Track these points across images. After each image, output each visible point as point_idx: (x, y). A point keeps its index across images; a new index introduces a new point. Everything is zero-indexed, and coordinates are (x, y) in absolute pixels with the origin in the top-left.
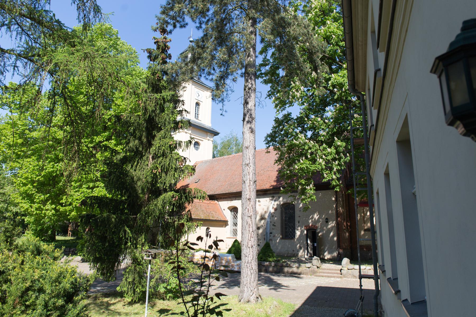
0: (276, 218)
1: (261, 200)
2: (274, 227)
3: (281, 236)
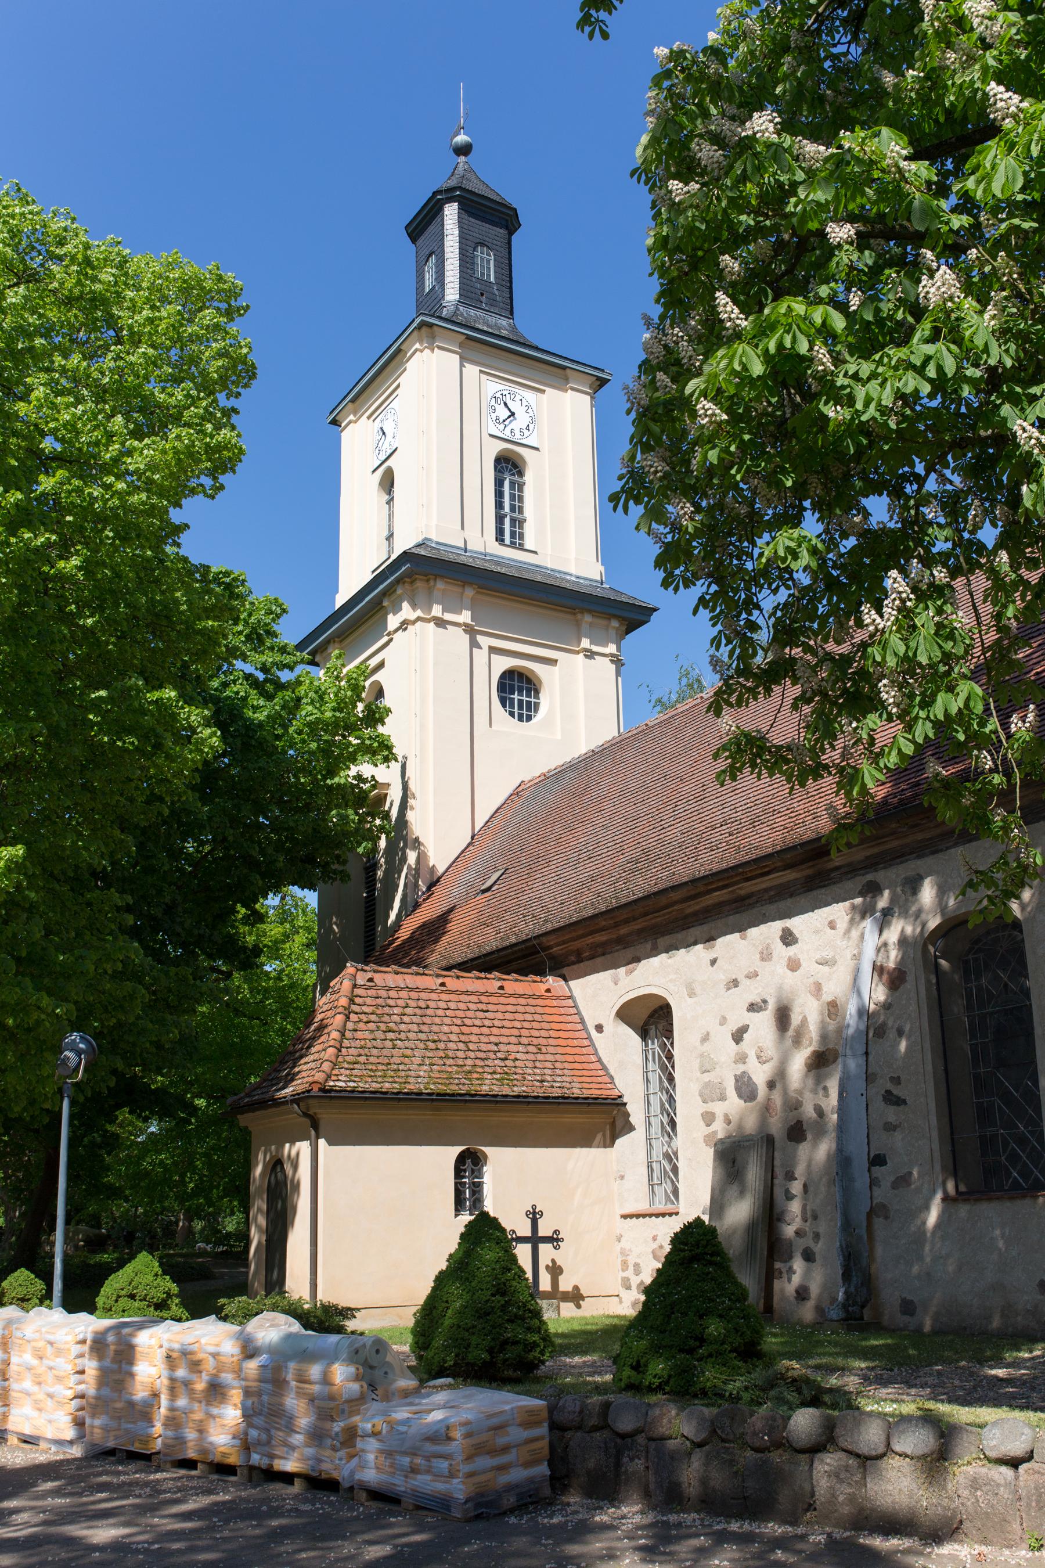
0: (903, 1046)
1: (797, 923)
2: (891, 1114)
3: (950, 1186)
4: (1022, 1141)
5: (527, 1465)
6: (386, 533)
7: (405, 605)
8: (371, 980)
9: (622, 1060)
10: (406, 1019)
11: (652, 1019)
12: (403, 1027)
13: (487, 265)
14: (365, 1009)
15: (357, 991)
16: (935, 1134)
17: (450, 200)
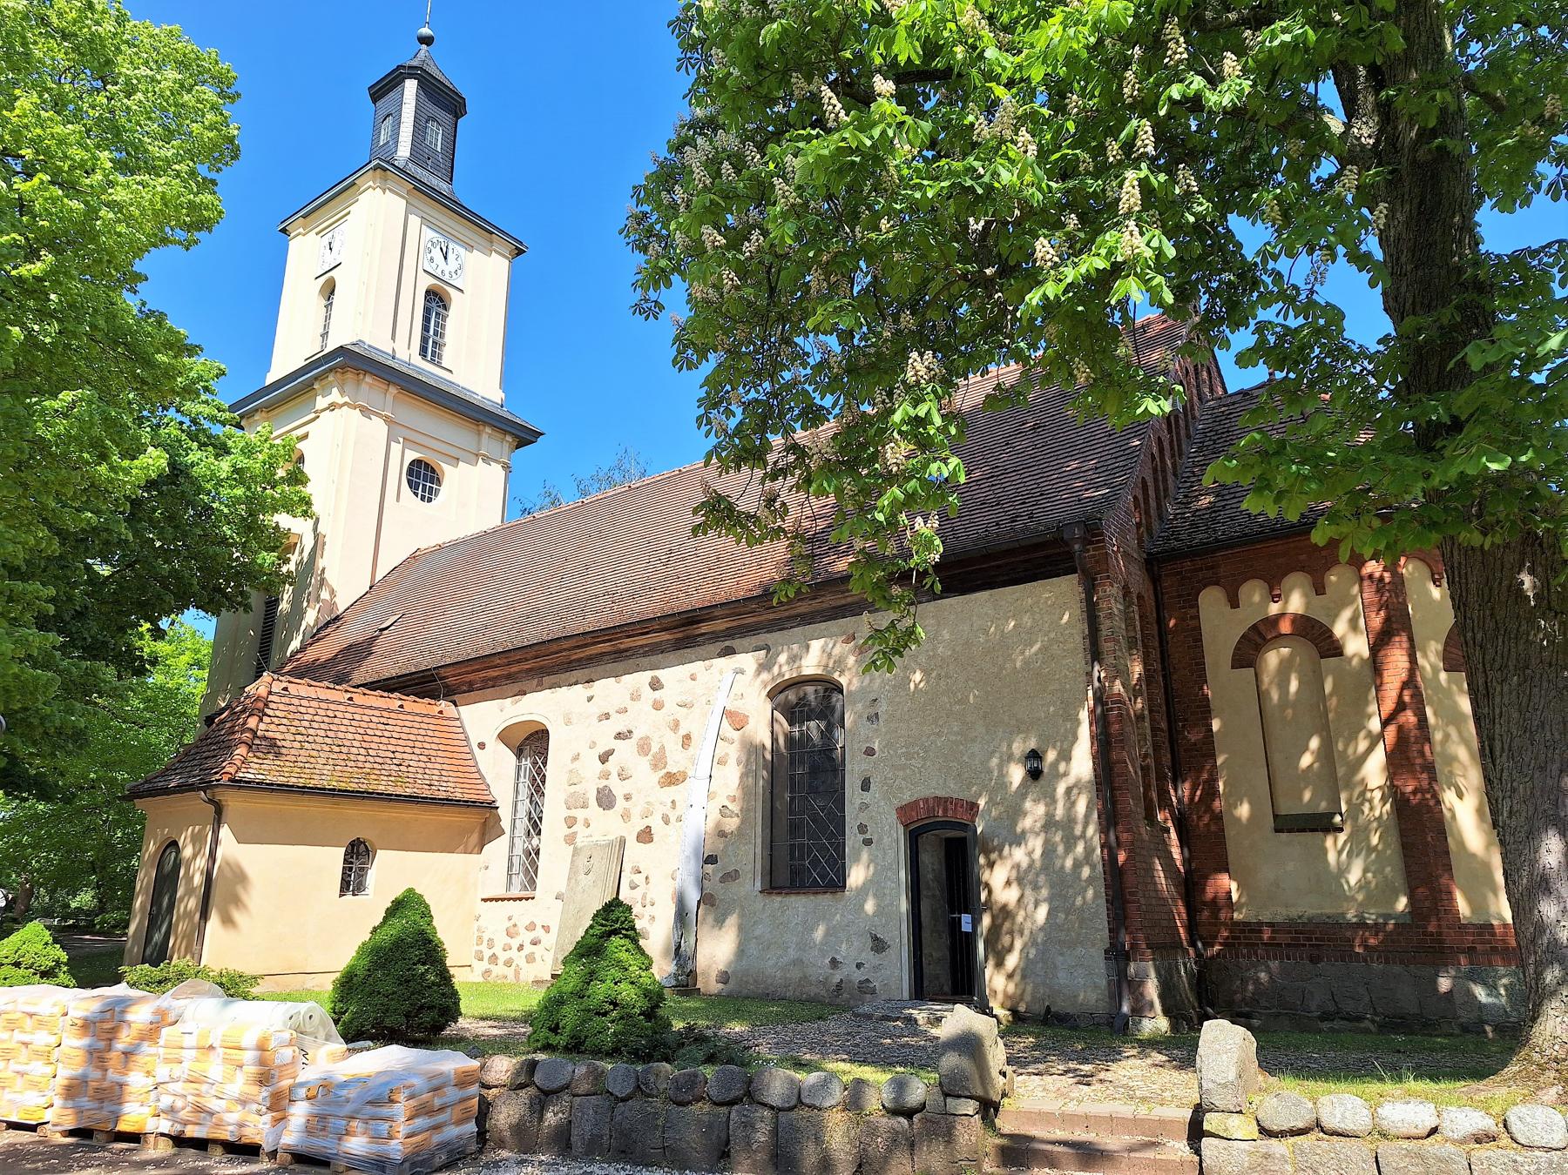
1: (661, 674)
4: (822, 849)
5: (459, 1122)
6: (321, 331)
7: (335, 390)
8: (285, 689)
9: (499, 773)
10: (315, 725)
11: (531, 743)
12: (311, 731)
13: (436, 138)
14: (278, 713)
15: (271, 698)
16: (759, 841)
17: (411, 76)
